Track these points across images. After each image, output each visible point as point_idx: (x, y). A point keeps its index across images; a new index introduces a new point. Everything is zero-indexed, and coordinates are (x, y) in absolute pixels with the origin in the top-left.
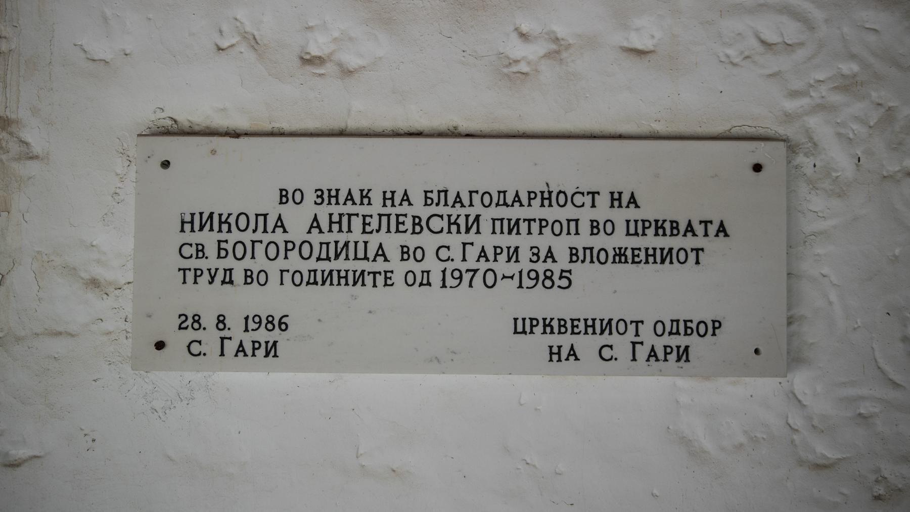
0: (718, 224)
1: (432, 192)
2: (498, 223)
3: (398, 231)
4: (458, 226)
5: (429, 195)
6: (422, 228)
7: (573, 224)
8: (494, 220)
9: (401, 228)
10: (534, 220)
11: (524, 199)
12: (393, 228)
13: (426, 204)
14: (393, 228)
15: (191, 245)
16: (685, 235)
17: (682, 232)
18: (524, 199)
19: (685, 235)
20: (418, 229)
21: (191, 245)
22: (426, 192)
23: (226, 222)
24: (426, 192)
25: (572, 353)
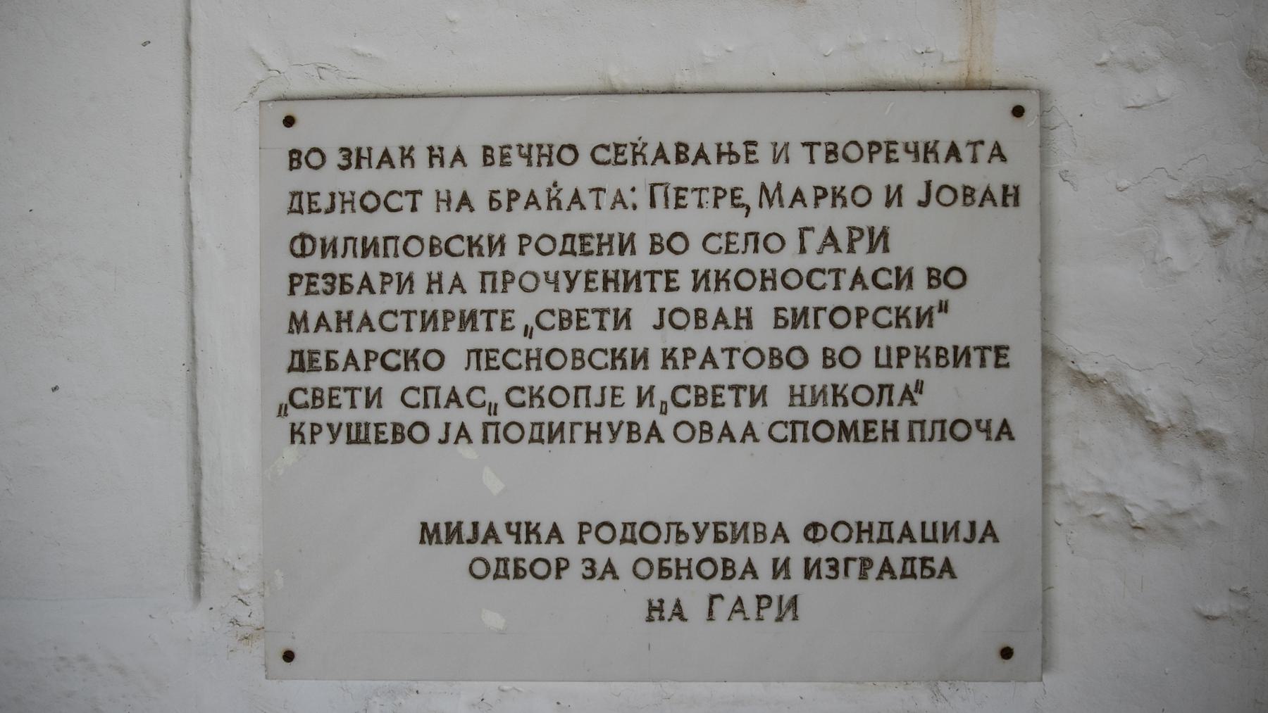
0: (614, 193)
1: (784, 309)
2: (489, 279)
3: (311, 211)
4: (302, 435)
5: (781, 313)
6: (300, 163)
7: (582, 393)
8: (484, 274)
9: (492, 364)
10: (496, 312)
11: (809, 196)
12: (483, 365)
13: (776, 326)
14: (483, 365)
15: (418, 390)
16: (648, 441)
17: (644, 437)
18: (809, 196)
19: (648, 441)
20: (399, 437)
21: (418, 390)
22: (777, 309)
23: (619, 358)
24: (777, 309)
25: (947, 567)
